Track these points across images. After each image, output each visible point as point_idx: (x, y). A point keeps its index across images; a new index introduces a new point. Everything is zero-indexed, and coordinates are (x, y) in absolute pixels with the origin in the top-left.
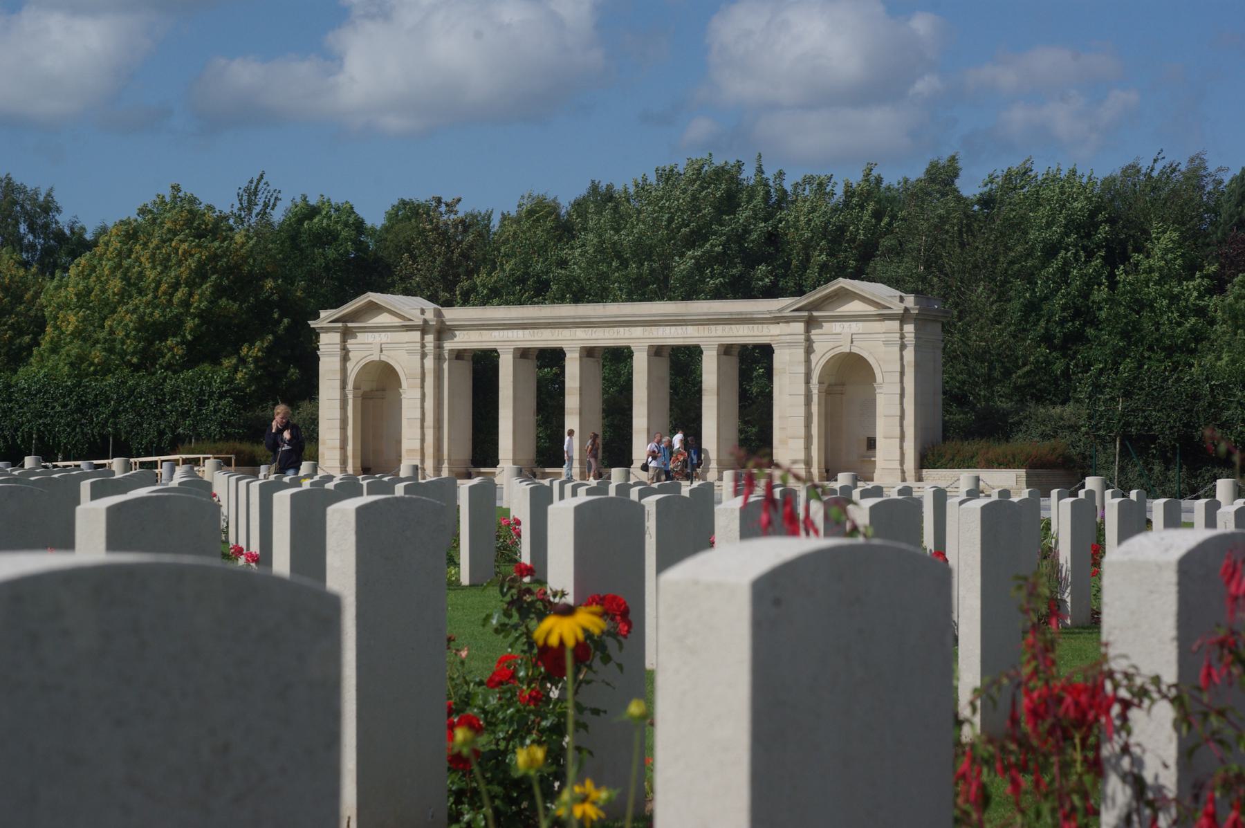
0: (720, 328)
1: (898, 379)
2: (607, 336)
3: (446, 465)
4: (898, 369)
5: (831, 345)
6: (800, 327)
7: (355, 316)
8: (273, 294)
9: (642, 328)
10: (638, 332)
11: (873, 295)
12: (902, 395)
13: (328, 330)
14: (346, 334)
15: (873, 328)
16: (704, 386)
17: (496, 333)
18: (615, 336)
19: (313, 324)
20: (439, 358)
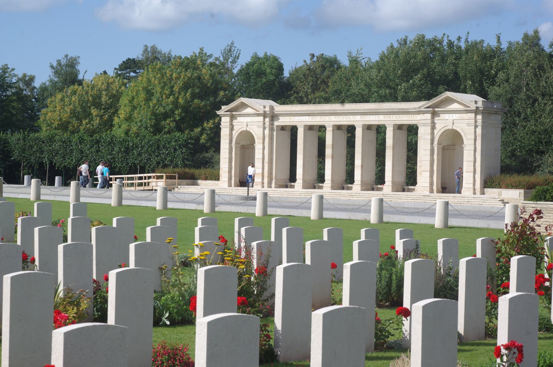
0: (394, 116)
1: (473, 143)
2: (345, 119)
3: (274, 181)
4: (473, 137)
5: (444, 125)
6: (429, 116)
7: (236, 109)
8: (223, 98)
9: (361, 115)
10: (358, 118)
11: (462, 100)
12: (475, 151)
13: (225, 115)
14: (233, 118)
15: (461, 116)
16: (387, 145)
17: (297, 118)
18: (348, 120)
19: (218, 113)
20: (271, 130)
